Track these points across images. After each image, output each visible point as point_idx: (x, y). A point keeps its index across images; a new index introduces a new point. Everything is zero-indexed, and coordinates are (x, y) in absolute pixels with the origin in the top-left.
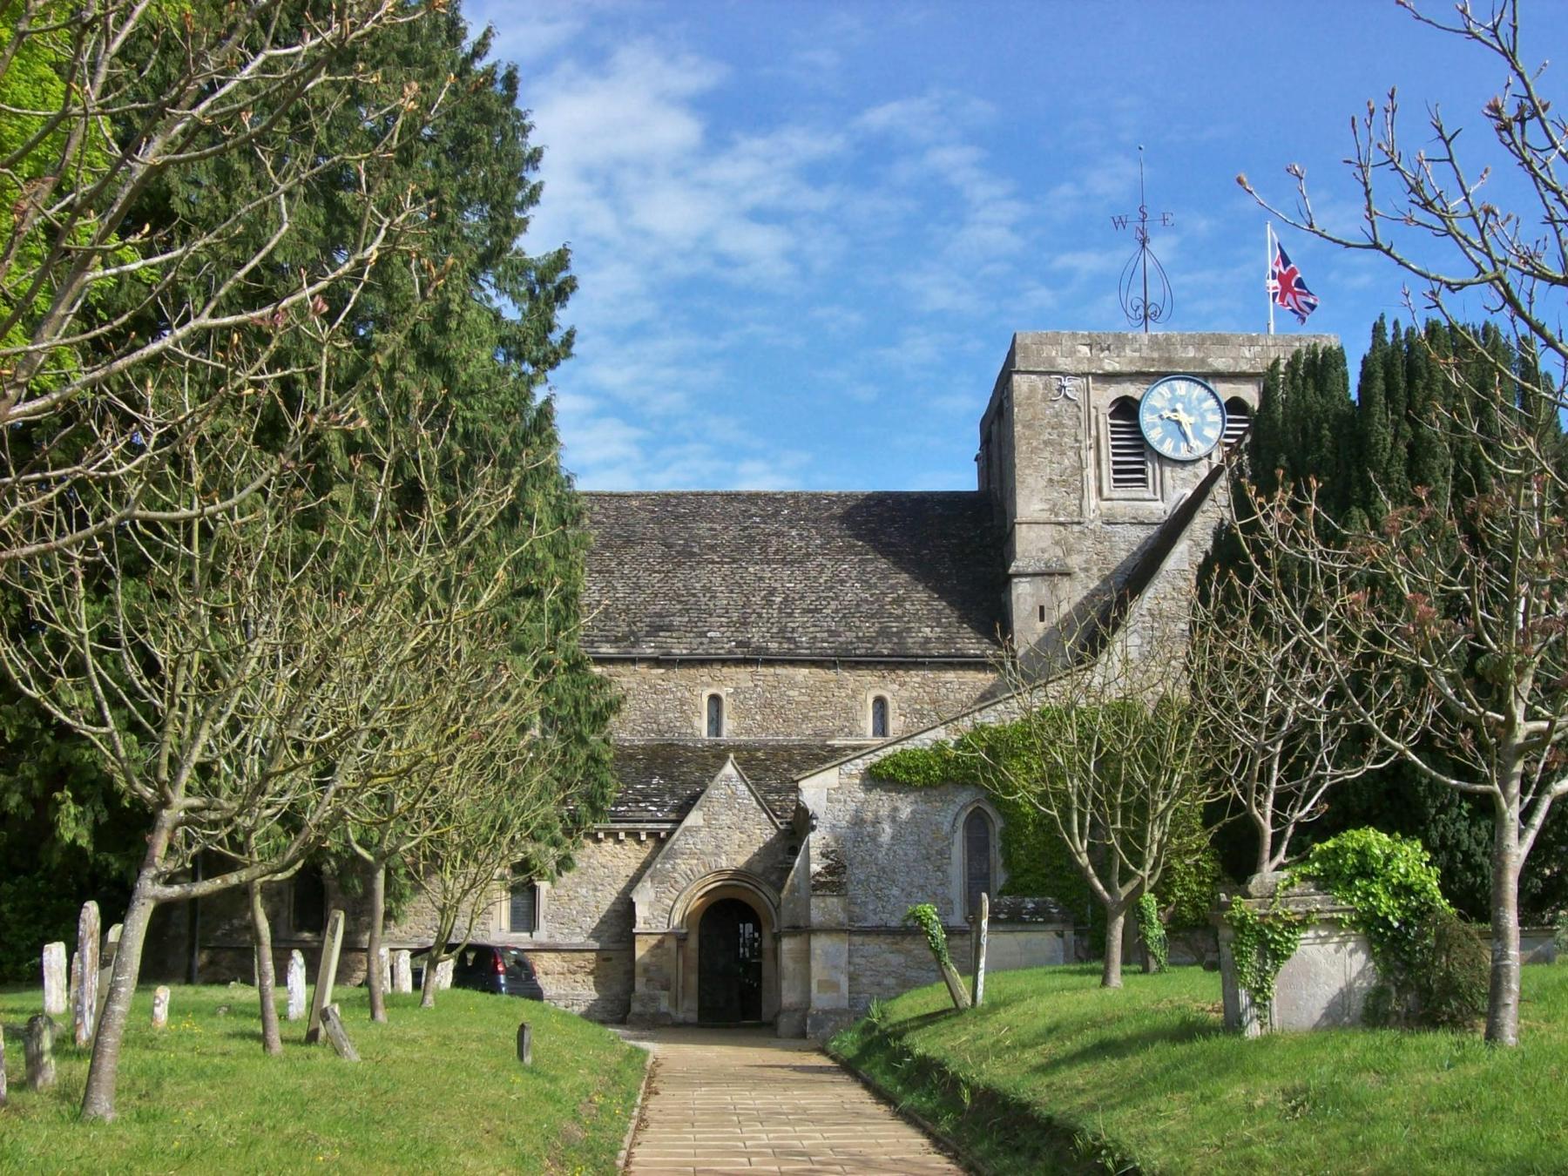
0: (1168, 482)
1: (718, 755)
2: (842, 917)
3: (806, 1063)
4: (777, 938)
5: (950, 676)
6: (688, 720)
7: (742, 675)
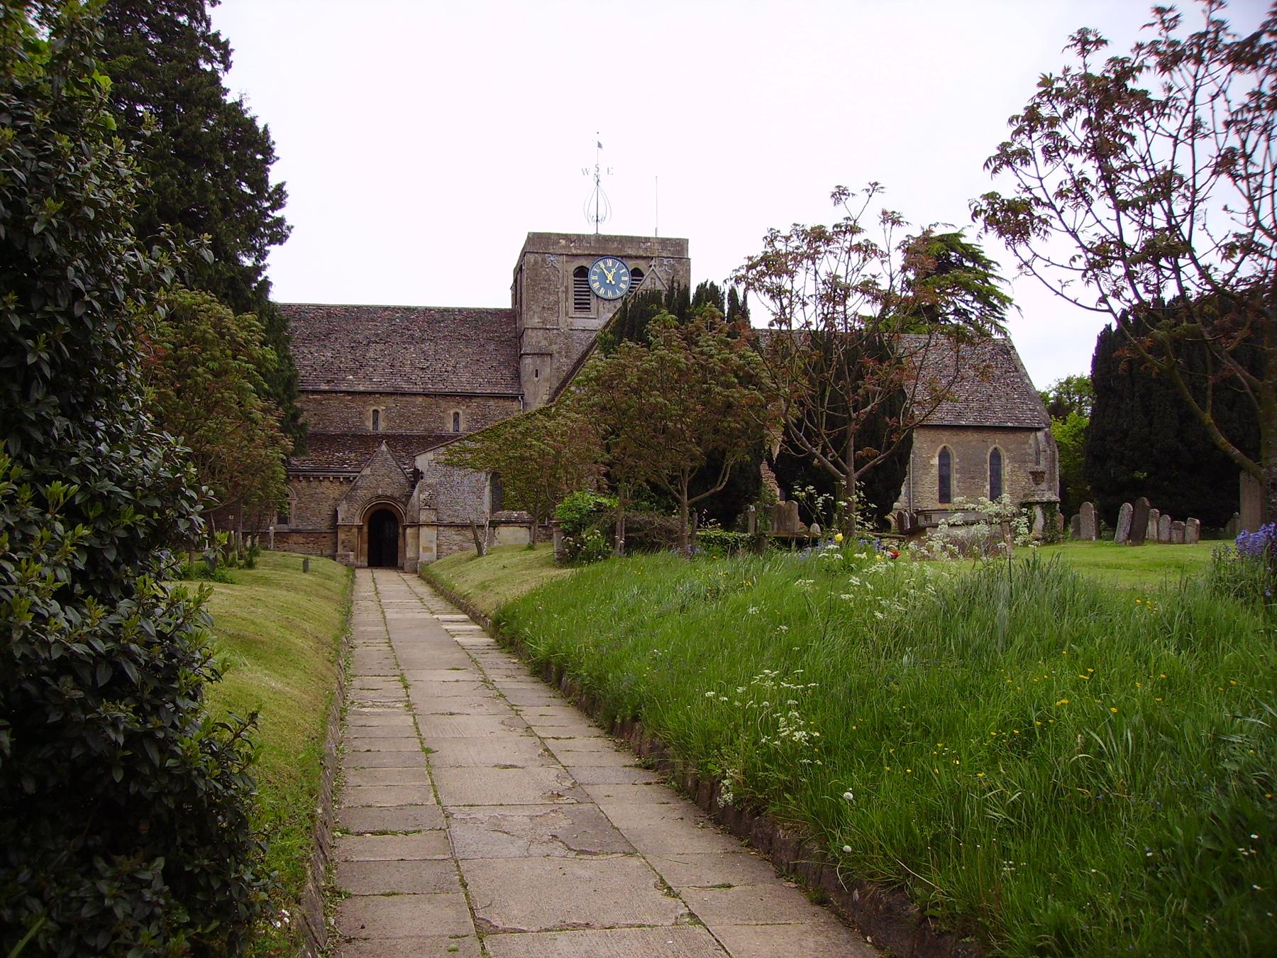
0: (601, 309)
1: (377, 439)
2: (434, 519)
3: (1099, 559)
4: (405, 528)
5: (491, 403)
6: (363, 422)
7: (390, 401)
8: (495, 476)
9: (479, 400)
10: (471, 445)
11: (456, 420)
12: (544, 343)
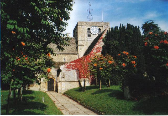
8: (78, 70)
9: (70, 55)
10: (72, 64)
11: (65, 59)
12: (82, 43)
